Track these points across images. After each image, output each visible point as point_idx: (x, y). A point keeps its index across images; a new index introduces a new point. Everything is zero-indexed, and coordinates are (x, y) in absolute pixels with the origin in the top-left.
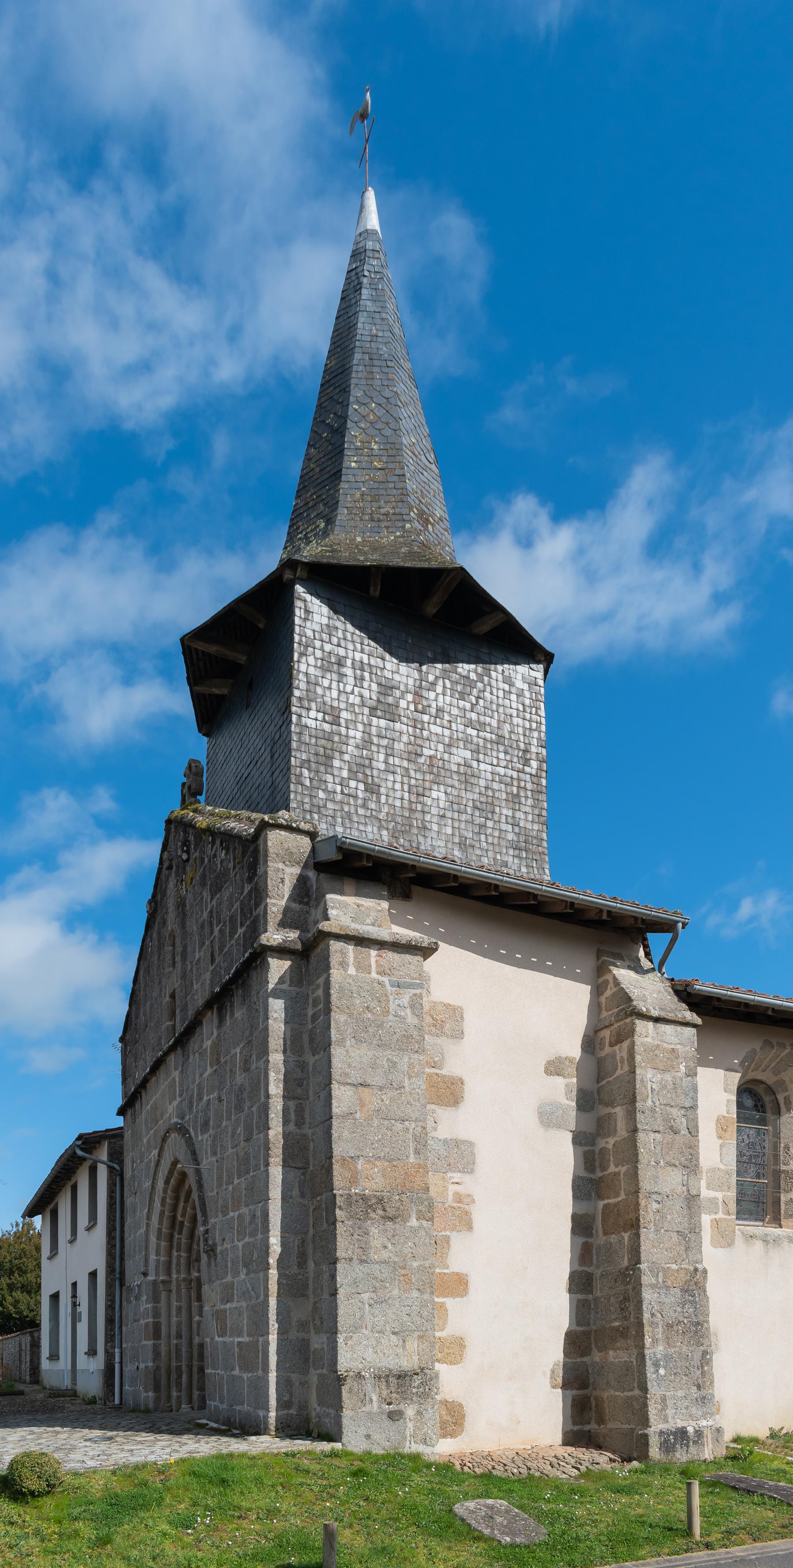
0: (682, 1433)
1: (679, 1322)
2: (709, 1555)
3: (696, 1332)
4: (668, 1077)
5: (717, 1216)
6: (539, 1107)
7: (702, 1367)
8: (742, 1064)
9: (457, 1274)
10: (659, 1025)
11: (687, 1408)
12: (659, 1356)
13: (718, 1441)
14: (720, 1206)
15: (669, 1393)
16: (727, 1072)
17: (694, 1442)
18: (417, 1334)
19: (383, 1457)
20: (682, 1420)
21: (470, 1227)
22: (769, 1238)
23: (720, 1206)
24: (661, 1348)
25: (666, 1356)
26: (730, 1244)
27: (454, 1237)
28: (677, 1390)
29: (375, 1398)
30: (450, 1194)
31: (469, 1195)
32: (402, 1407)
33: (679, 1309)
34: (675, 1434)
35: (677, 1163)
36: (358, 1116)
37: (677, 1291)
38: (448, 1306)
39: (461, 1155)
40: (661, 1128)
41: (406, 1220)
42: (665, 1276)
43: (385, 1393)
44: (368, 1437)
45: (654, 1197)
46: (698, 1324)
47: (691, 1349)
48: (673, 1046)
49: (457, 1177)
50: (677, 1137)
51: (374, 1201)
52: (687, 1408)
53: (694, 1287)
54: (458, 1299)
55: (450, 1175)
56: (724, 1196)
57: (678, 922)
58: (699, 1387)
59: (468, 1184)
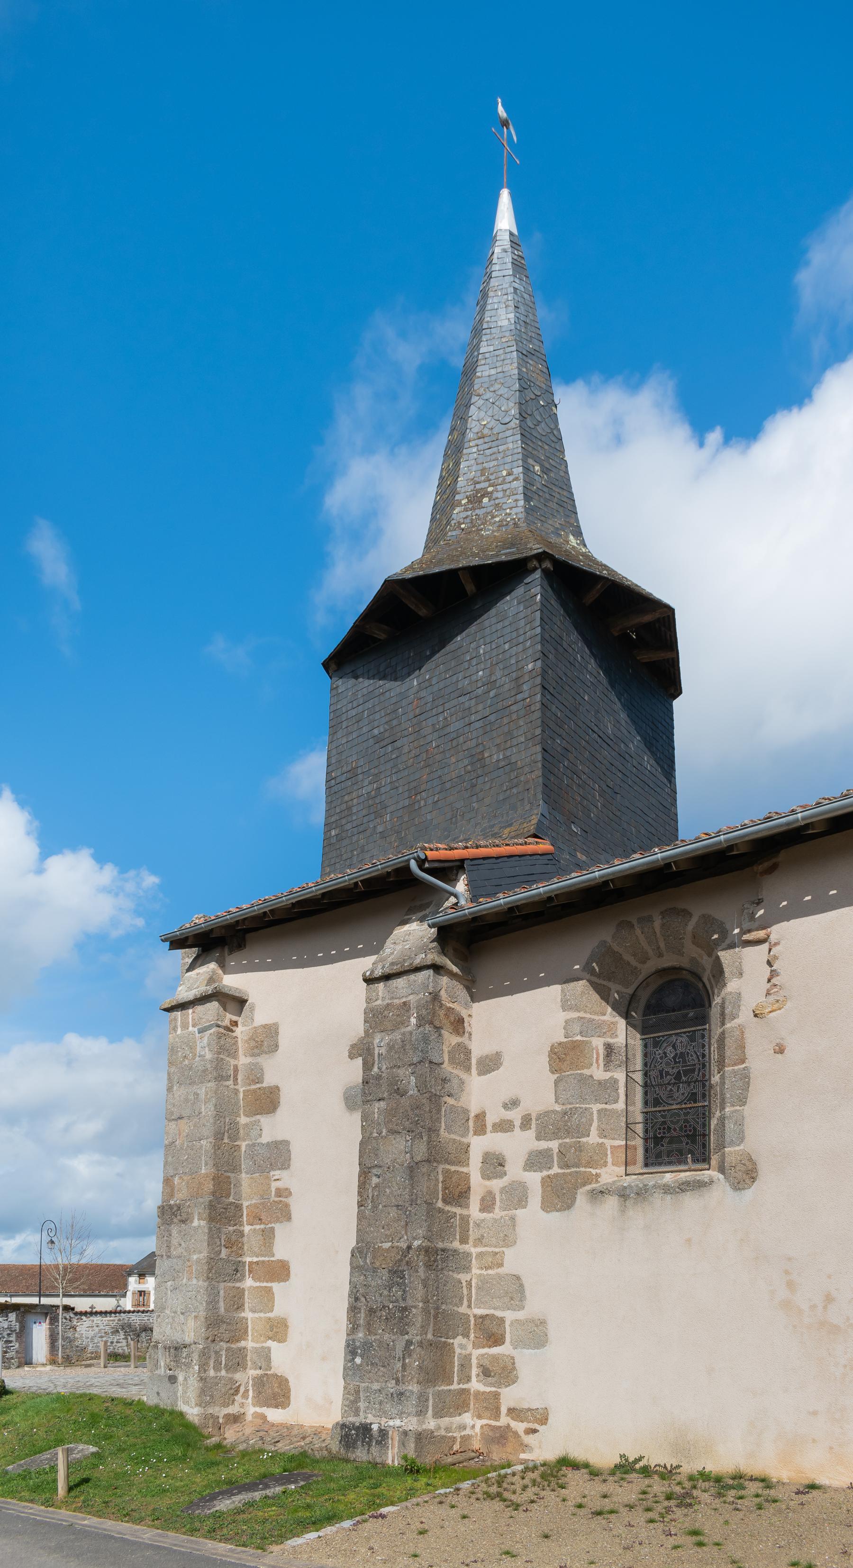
0: (365, 1429)
1: (384, 1307)
2: (188, 1541)
3: (402, 1318)
4: (397, 1035)
5: (551, 1172)
6: (345, 1093)
7: (404, 1358)
8: (587, 967)
9: (281, 1261)
10: (390, 982)
11: (381, 1403)
12: (358, 1344)
13: (403, 1444)
14: (555, 1159)
15: (363, 1385)
16: (564, 986)
17: (377, 1441)
18: (194, 1314)
19: (150, 1409)
20: (374, 1416)
21: (289, 1218)
22: (628, 1192)
23: (555, 1159)
24: (361, 1335)
25: (365, 1343)
26: (568, 1205)
27: (277, 1227)
28: (372, 1382)
29: (162, 1364)
30: (273, 1190)
31: (287, 1189)
32: (176, 1373)
33: (386, 1293)
34: (357, 1429)
35: (400, 1128)
36: (177, 1143)
37: (385, 1272)
38: (274, 1290)
39: (279, 1155)
40: (386, 1095)
41: (192, 1222)
42: (374, 1257)
43: (168, 1360)
44: (158, 1393)
45: (375, 1171)
46: (405, 1309)
47: (393, 1337)
48: (404, 1000)
49: (276, 1174)
50: (403, 1100)
51: (175, 1209)
52: (381, 1403)
53: (405, 1268)
54: (282, 1284)
55: (272, 1173)
56: (560, 1145)
57: (408, 861)
58: (398, 1382)
59: (282, 1179)
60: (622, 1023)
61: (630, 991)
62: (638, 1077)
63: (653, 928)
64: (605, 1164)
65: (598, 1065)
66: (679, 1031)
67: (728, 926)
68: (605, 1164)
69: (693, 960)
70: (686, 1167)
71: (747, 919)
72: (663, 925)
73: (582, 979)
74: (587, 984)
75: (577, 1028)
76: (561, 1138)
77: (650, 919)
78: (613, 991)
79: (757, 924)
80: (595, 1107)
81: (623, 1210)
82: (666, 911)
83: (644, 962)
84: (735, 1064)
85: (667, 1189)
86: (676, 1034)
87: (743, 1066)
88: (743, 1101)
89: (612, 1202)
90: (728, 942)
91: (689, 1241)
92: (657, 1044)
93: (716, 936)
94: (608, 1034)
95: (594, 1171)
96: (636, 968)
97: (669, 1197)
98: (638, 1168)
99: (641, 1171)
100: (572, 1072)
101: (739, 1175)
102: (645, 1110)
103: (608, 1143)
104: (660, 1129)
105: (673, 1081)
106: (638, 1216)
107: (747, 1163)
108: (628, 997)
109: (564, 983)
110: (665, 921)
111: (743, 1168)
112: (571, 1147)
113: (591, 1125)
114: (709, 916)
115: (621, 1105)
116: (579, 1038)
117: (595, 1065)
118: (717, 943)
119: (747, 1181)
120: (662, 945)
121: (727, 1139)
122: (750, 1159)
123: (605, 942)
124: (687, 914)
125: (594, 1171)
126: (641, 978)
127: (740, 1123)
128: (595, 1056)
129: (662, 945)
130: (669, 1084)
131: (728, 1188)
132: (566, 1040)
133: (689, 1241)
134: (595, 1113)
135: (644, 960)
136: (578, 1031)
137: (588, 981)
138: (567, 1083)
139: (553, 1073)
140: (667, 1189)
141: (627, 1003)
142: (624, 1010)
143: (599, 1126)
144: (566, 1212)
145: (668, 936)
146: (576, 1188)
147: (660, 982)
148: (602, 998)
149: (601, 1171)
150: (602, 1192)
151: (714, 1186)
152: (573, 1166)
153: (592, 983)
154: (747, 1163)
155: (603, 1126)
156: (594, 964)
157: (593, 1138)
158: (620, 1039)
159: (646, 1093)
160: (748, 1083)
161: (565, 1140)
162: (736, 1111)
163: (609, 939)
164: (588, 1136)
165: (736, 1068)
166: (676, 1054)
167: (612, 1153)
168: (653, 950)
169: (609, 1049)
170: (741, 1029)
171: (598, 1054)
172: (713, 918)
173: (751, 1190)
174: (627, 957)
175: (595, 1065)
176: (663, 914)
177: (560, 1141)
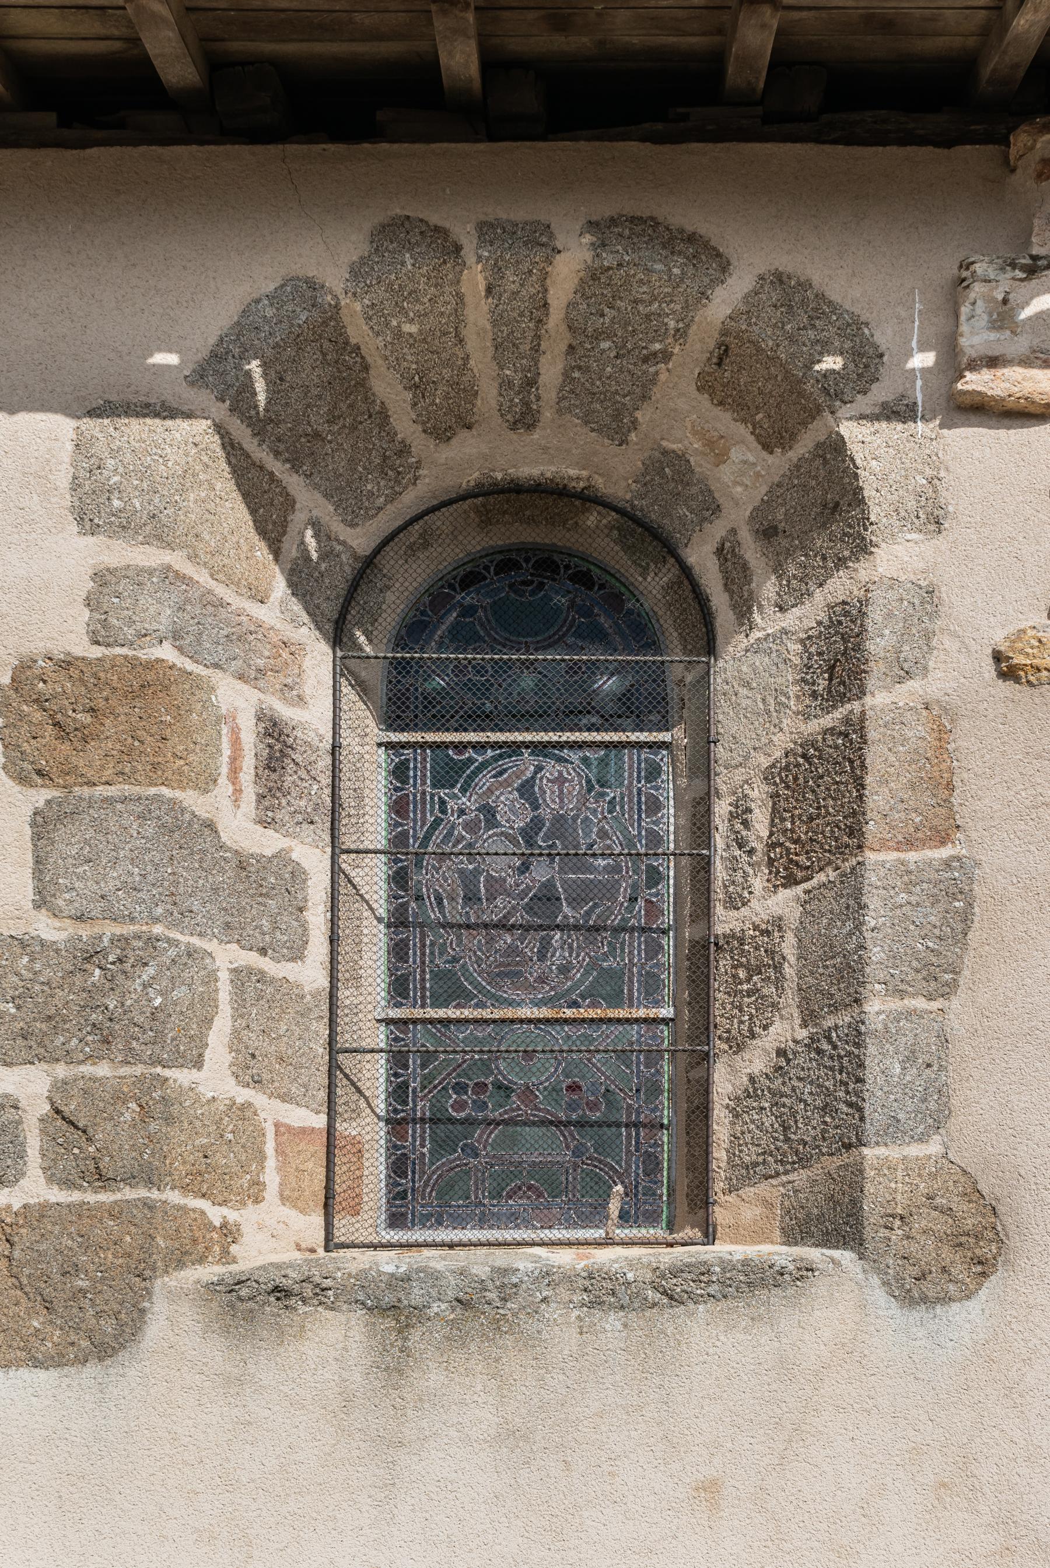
16: (89, 425)
22: (417, 1295)
56: (61, 1086)
60: (318, 658)
61: (360, 539)
62: (373, 877)
63: (545, 276)
64: (255, 1194)
65: (238, 791)
66: (553, 736)
67: (883, 337)
68: (255, 1194)
69: (670, 470)
70: (599, 1233)
71: (983, 320)
72: (593, 276)
73: (189, 415)
74: (214, 442)
75: (158, 612)
76: (68, 1057)
77: (539, 239)
78: (299, 517)
79: (1022, 345)
80: (227, 957)
81: (394, 1367)
82: (613, 221)
83: (442, 434)
84: (909, 844)
85: (601, 1293)
86: (540, 749)
87: (945, 852)
88: (940, 978)
89: (336, 1339)
90: (881, 393)
91: (710, 1490)
92: (450, 772)
93: (832, 363)
94: (276, 681)
95: (216, 1214)
96: (404, 450)
97: (613, 1321)
98: (368, 1220)
99: (374, 1239)
100: (128, 789)
101: (925, 1249)
102: (394, 1013)
103: (270, 1111)
104: (460, 1088)
105: (804, 818)
106: (462, 1394)
107: (961, 1207)
108: (348, 568)
109: (94, 413)
110: (609, 260)
111: (942, 1225)
112: (120, 1098)
113: (208, 1022)
114: (805, 285)
115: (311, 973)
116: (167, 652)
117: (224, 787)
118: (835, 392)
119: (958, 1270)
120: (551, 371)
121: (875, 1117)
122: (974, 1193)
123: (313, 285)
124: (709, 258)
125: (216, 1214)
126: (411, 500)
127: (932, 1059)
128: (227, 752)
129: (551, 371)
130: (503, 926)
131: (879, 1296)
132: (97, 652)
133: (710, 1490)
134: (224, 976)
135: (449, 423)
136: (163, 624)
137: (219, 429)
138: (99, 827)
139: (22, 779)
140: (601, 1293)
141: (342, 587)
142: (331, 609)
143: (236, 1033)
144: (92, 1369)
145: (598, 336)
146: (143, 1273)
147: (477, 542)
148: (262, 531)
149: (245, 1217)
150: (280, 1292)
151: (819, 1287)
152: (131, 1180)
153: (231, 446)
154: (961, 1207)
155: (253, 1039)
156: (254, 366)
157: (214, 1079)
158: (312, 717)
159: (398, 951)
160: (966, 918)
161: (86, 1069)
162: (910, 1014)
163: (335, 279)
164: (198, 1063)
165: (912, 856)
166: (536, 824)
167: (279, 1151)
168: (506, 384)
169: (275, 734)
170: (941, 720)
171: (236, 743)
172: (820, 296)
173: (973, 1306)
174: (387, 388)
175: (224, 787)
176: (601, 229)
177: (61, 1070)
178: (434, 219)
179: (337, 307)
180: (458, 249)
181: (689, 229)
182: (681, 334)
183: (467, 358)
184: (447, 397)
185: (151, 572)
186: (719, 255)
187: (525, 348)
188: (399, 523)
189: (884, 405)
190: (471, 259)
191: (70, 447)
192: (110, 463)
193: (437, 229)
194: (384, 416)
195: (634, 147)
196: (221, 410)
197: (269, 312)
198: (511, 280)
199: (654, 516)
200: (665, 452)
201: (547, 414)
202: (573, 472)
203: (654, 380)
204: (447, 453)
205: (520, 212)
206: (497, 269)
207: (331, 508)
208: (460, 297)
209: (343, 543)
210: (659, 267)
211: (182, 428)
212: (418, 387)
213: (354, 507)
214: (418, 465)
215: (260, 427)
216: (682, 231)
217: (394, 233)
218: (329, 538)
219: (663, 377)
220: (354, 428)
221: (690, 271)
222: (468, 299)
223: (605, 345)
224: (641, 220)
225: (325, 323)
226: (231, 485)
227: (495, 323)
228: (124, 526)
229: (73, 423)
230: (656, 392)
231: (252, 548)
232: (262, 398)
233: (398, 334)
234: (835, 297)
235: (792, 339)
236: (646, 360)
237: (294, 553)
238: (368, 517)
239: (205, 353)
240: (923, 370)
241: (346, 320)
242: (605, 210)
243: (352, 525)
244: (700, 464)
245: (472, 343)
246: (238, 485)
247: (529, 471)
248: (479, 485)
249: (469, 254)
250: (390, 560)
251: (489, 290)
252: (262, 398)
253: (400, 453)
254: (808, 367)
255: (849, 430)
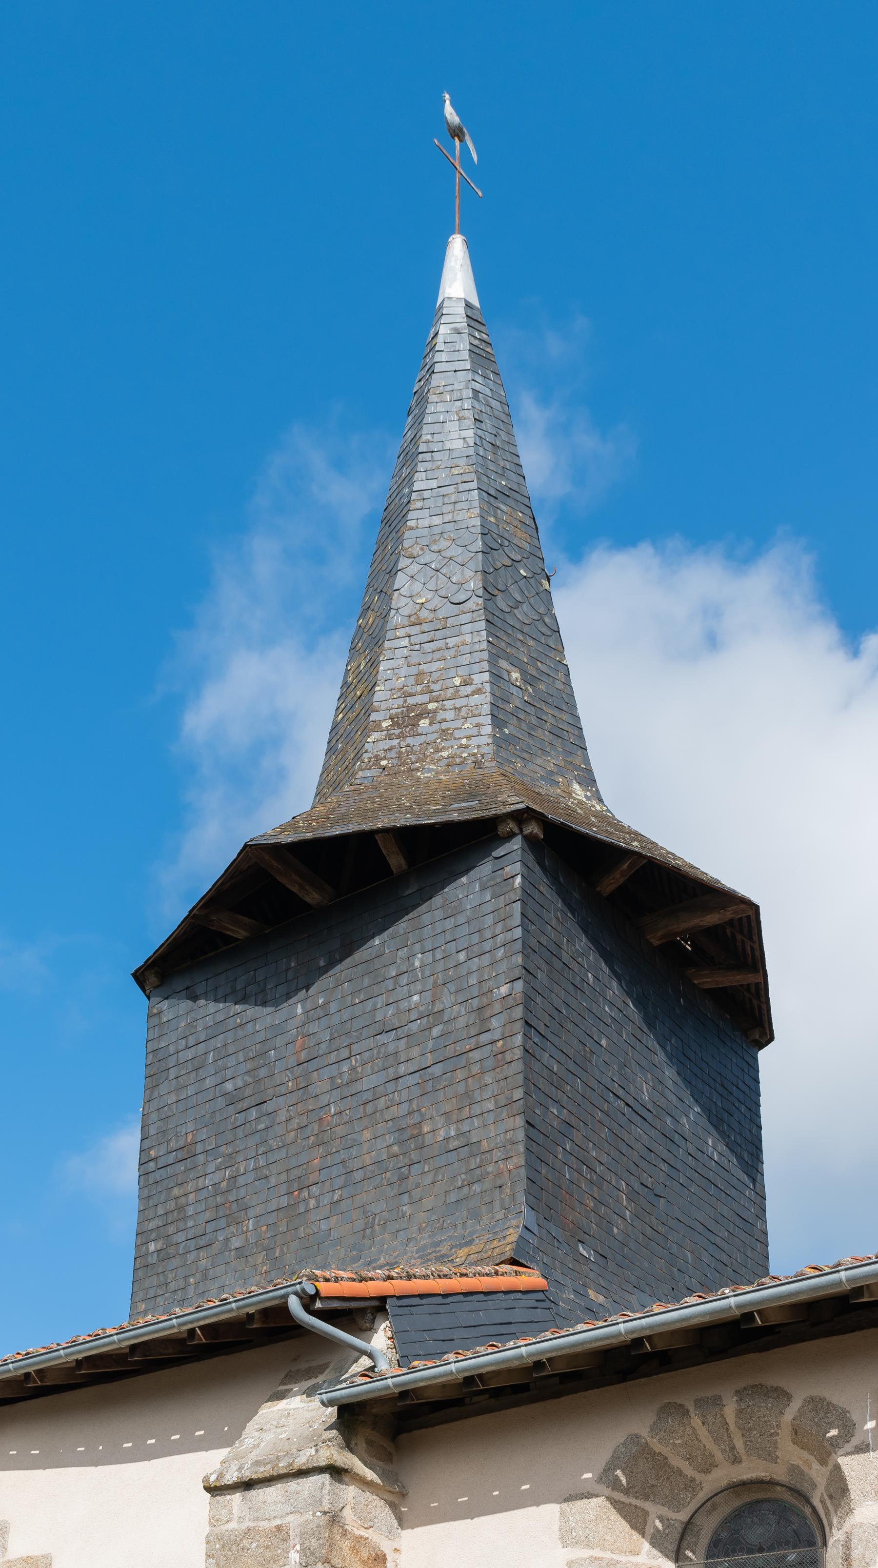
16: (565, 1506)
61: (683, 1516)
67: (855, 1417)
73: (597, 1496)
74: (607, 1504)
77: (717, 1402)
83: (707, 1471)
90: (855, 1441)
93: (834, 1432)
108: (679, 1527)
109: (566, 1500)
110: (743, 1406)
114: (822, 1399)
118: (835, 1444)
123: (637, 1436)
126: (702, 1496)
135: (708, 1466)
137: (608, 1498)
141: (678, 1536)
142: (673, 1547)
145: (750, 1430)
147: (737, 1503)
148: (634, 1527)
153: (614, 1503)
156: (619, 1472)
163: (644, 1432)
172: (829, 1403)
176: (740, 1394)
178: (679, 1402)
179: (647, 1443)
180: (688, 1411)
181: (775, 1385)
182: (778, 1426)
183: (705, 1446)
184: (703, 1459)
185: (585, 1559)
186: (788, 1394)
187: (725, 1438)
188: (699, 1505)
189: (856, 1447)
190: (693, 1415)
191: (558, 1514)
192: (571, 1518)
193: (680, 1405)
194: (680, 1472)
195: (752, 1356)
196: (608, 1491)
197: (623, 1450)
198: (710, 1419)
199: (799, 1487)
200: (792, 1465)
201: (744, 1457)
202: (763, 1474)
203: (776, 1442)
204: (710, 1477)
205: (709, 1393)
206: (703, 1416)
207: (667, 1509)
208: (694, 1428)
209: (676, 1520)
210: (763, 1405)
211: (594, 1501)
212: (690, 1459)
213: (675, 1504)
214: (701, 1483)
215: (627, 1491)
216: (771, 1387)
217: (666, 1410)
218: (668, 1520)
219: (779, 1440)
220: (668, 1479)
221: (776, 1403)
222: (697, 1428)
223: (754, 1432)
224: (756, 1386)
225: (643, 1449)
226: (618, 1516)
227: (710, 1433)
228: (577, 1543)
229: (559, 1506)
230: (780, 1446)
231: (631, 1536)
232: (624, 1481)
233: (674, 1445)
234: (835, 1402)
235: (818, 1425)
236: (771, 1435)
237: (652, 1531)
238: (684, 1507)
239: (602, 1470)
240: (872, 1429)
241: (652, 1446)
242: (741, 1385)
243: (678, 1512)
244: (805, 1469)
245: (704, 1441)
246: (621, 1515)
247: (746, 1476)
248: (728, 1484)
249: (692, 1413)
250: (699, 1520)
251: (703, 1423)
252: (624, 1481)
253: (691, 1481)
254: (825, 1436)
255: (842, 1461)
